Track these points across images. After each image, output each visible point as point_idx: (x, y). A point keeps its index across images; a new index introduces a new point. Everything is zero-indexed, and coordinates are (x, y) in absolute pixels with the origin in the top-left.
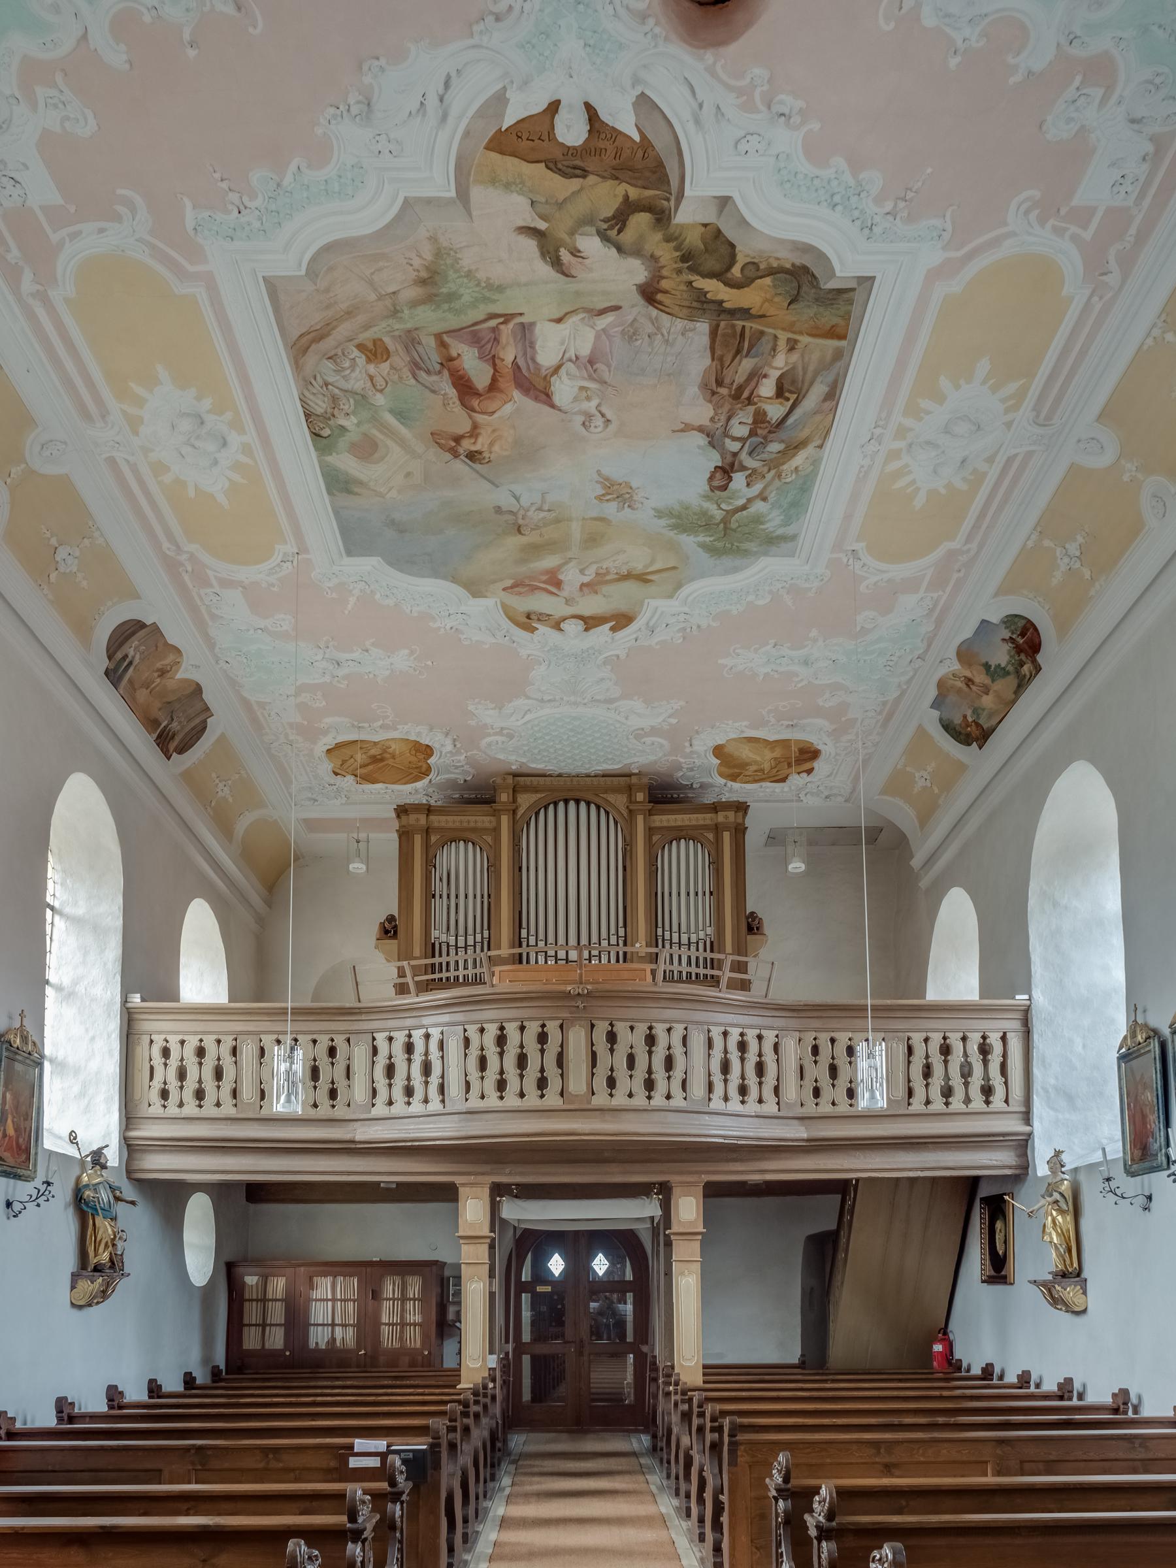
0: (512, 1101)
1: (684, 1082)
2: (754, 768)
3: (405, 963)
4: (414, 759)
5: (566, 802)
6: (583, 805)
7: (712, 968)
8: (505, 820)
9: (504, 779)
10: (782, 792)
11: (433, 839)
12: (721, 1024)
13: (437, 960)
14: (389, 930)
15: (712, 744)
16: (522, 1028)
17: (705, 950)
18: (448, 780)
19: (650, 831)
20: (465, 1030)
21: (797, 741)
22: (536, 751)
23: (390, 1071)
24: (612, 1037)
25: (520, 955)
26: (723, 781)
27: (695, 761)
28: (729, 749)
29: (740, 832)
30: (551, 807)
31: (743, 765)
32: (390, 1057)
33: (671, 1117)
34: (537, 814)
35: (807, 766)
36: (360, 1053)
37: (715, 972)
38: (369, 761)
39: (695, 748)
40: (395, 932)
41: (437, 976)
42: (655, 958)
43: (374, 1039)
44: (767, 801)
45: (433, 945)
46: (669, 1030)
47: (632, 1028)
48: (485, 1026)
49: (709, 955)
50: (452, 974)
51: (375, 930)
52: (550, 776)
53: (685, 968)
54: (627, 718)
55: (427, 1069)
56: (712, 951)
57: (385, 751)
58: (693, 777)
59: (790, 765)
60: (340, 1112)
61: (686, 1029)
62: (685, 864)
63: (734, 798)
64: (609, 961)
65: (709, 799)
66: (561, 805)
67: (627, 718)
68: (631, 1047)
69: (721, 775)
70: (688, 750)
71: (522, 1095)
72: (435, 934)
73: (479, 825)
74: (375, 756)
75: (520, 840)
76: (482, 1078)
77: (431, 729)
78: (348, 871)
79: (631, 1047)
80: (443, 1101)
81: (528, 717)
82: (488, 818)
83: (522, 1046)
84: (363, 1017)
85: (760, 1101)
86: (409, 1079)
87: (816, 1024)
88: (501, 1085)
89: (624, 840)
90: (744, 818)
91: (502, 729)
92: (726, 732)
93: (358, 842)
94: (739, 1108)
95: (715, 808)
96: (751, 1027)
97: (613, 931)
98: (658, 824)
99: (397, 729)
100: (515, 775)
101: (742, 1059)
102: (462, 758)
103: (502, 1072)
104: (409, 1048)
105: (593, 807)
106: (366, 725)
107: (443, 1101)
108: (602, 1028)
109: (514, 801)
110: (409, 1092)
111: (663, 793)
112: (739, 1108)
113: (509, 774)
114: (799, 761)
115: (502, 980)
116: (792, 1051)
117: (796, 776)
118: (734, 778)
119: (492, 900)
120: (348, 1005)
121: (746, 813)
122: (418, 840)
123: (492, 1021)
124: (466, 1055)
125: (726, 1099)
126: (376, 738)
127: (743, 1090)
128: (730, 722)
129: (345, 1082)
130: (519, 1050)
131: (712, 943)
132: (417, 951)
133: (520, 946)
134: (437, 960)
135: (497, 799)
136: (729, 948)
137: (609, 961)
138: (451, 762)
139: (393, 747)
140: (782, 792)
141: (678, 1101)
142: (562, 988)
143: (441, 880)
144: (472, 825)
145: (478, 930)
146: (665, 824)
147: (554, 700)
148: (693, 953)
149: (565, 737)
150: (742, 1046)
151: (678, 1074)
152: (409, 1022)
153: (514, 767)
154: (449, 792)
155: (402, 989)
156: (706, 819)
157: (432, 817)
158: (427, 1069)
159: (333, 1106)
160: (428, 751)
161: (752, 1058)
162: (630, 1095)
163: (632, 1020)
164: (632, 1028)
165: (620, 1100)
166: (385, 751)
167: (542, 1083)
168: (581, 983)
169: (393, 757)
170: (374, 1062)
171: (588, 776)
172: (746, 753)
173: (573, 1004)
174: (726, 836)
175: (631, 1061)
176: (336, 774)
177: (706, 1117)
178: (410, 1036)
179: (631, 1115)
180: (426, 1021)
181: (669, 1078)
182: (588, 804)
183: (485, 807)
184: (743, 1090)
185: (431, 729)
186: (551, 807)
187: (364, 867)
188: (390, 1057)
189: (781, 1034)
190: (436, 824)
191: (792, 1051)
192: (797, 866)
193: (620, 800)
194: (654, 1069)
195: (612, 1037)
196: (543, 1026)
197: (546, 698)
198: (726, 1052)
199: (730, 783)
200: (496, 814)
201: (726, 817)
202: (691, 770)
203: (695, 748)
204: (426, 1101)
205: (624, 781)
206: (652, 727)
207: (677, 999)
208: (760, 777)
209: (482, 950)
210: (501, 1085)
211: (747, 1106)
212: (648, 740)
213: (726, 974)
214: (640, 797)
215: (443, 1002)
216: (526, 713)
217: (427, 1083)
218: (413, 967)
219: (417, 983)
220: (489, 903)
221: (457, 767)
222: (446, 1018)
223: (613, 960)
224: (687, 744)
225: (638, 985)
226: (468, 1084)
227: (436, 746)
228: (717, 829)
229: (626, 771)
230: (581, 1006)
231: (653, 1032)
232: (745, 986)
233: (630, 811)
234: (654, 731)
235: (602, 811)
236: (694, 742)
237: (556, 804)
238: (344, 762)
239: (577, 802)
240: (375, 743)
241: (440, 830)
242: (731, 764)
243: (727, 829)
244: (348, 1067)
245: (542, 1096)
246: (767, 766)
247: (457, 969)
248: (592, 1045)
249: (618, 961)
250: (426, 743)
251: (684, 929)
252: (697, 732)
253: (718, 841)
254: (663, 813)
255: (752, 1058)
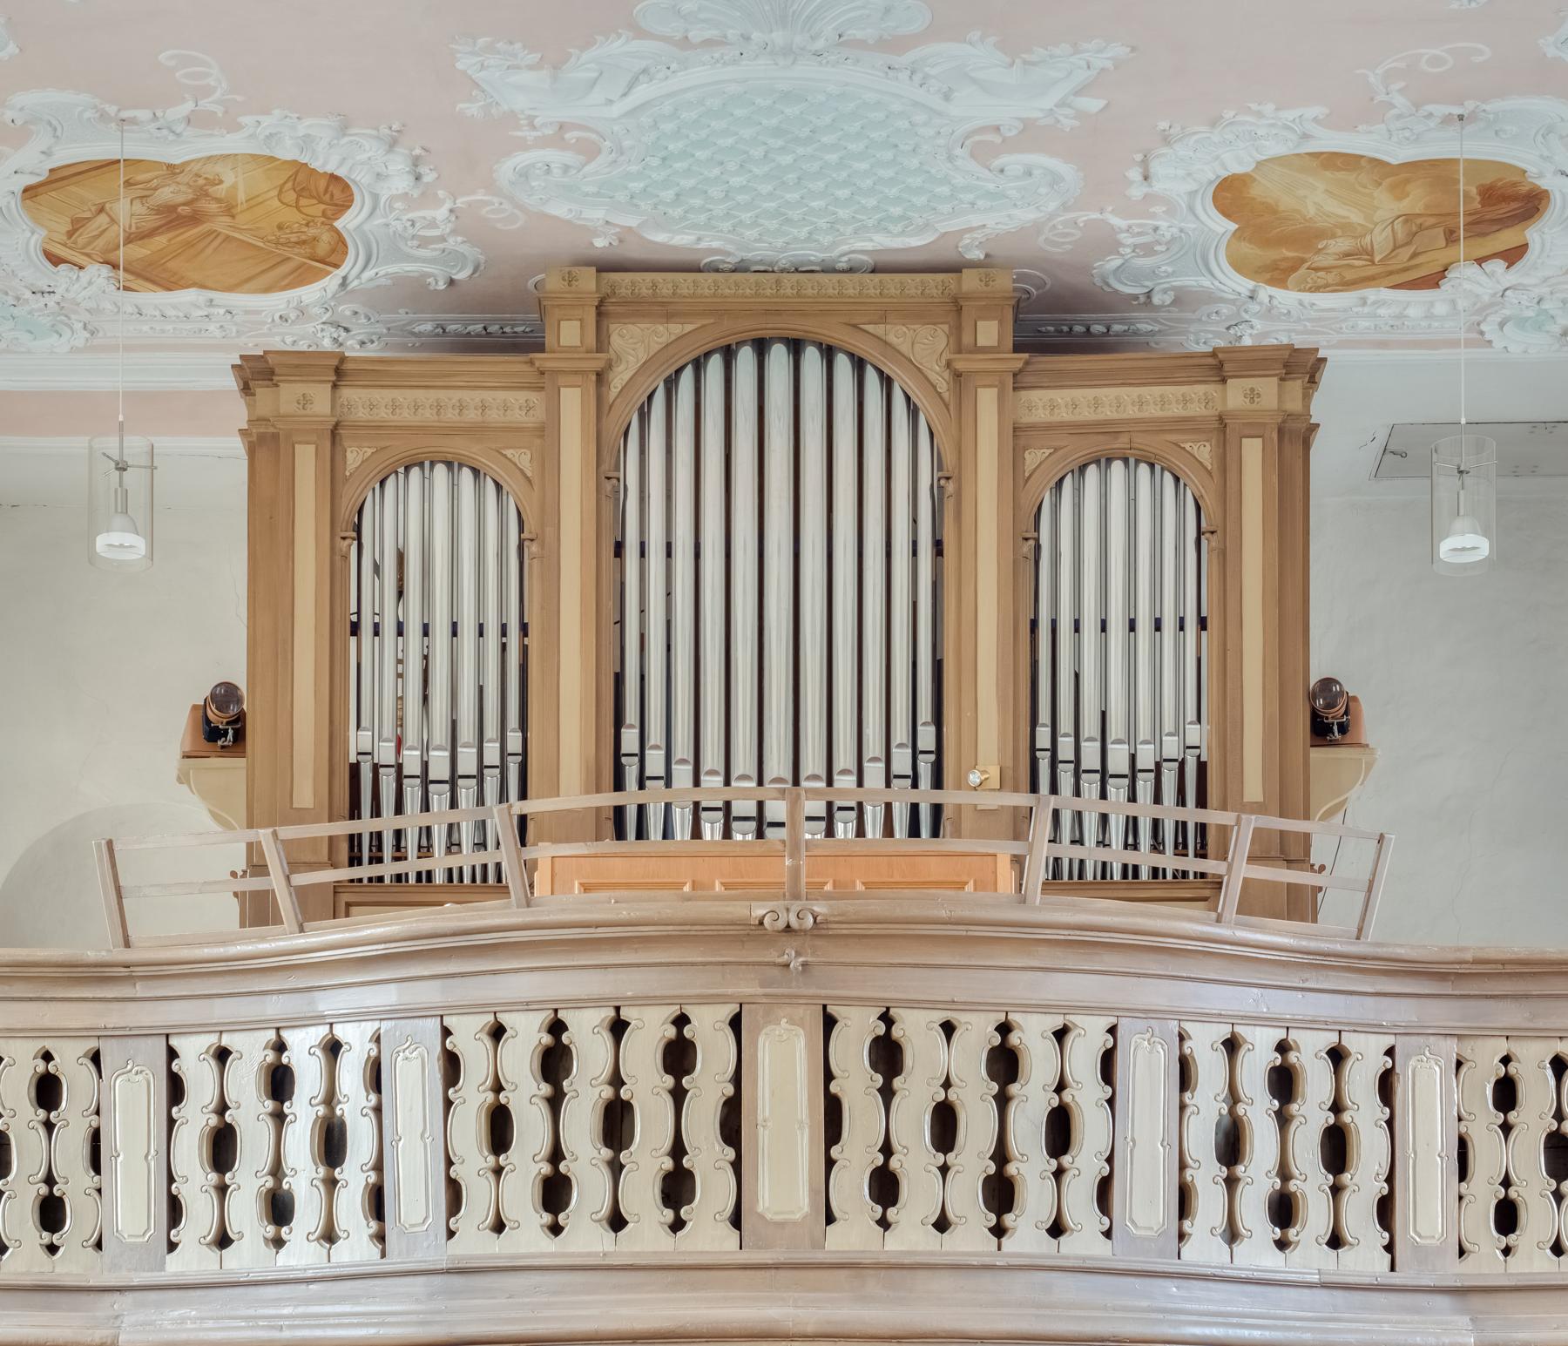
0: (584, 1231)
1: (1104, 1189)
2: (1343, 244)
3: (263, 835)
4: (291, 216)
5: (761, 347)
6: (812, 359)
7: (1202, 854)
8: (573, 403)
9: (570, 279)
10: (1429, 316)
11: (354, 457)
12: (1218, 1018)
13: (365, 825)
14: (222, 728)
15: (1211, 173)
16: (618, 1028)
17: (1181, 801)
18: (399, 281)
19: (1018, 436)
20: (446, 1032)
21: (1473, 165)
22: (668, 195)
23: (222, 1147)
24: (887, 1056)
25: (619, 811)
26: (1244, 285)
27: (1156, 226)
28: (1266, 190)
29: (1294, 440)
30: (715, 365)
31: (1309, 237)
32: (222, 1108)
33: (1067, 1287)
34: (671, 384)
35: (1507, 239)
36: (131, 1098)
37: (1210, 866)
38: (152, 221)
39: (1158, 186)
40: (240, 736)
41: (365, 871)
42: (1019, 824)
43: (172, 1054)
44: (1383, 345)
45: (355, 770)
46: (1061, 1035)
47: (948, 1028)
48: (505, 1019)
49: (1192, 815)
50: (412, 865)
51: (178, 728)
52: (715, 269)
53: (1117, 856)
54: (947, 97)
55: (332, 1143)
56: (1202, 802)
57: (202, 193)
58: (1153, 273)
59: (1451, 237)
60: (74, 1263)
61: (1112, 1031)
62: (1122, 540)
63: (1282, 336)
64: (860, 832)
65: (1202, 339)
66: (745, 359)
67: (947, 97)
68: (947, 1085)
69: (1240, 266)
70: (1137, 192)
71: (617, 1222)
72: (358, 740)
73: (494, 416)
74: (171, 208)
75: (619, 464)
76: (498, 1171)
77: (344, 129)
78: (92, 558)
79: (947, 1085)
80: (380, 1237)
81: (642, 92)
82: (521, 396)
83: (617, 1081)
84: (140, 990)
85: (1335, 1241)
86: (277, 1171)
87: (1511, 1015)
88: (555, 1193)
89: (938, 462)
90: (1307, 398)
91: (562, 127)
92: (1254, 139)
93: (122, 468)
94: (1271, 1261)
95: (1218, 367)
96: (1312, 1025)
97: (901, 733)
98: (1040, 416)
99: (235, 127)
100: (605, 267)
101: (1283, 1119)
102: (441, 213)
103: (556, 1155)
104: (279, 1082)
105: (843, 365)
106: (143, 114)
107: (380, 1237)
108: (857, 1030)
109: (602, 344)
110: (279, 1209)
111: (1058, 324)
112: (1271, 1261)
113: (588, 263)
114: (1479, 226)
115: (568, 881)
116: (1436, 1099)
117: (1472, 270)
118: (1279, 274)
119: (533, 641)
120: (91, 955)
121: (1313, 381)
122: (307, 462)
123: (527, 1006)
124: (448, 1104)
125: (1232, 1235)
126: (176, 154)
127: (1283, 1210)
128: (1269, 108)
129: (88, 1179)
130: (608, 1092)
131: (1202, 767)
132: (306, 794)
133: (619, 785)
134: (365, 825)
135: (549, 341)
136: (1253, 790)
137: (860, 832)
138: (409, 229)
139: (229, 179)
140: (1429, 316)
141: (1085, 1240)
142: (737, 910)
143: (377, 569)
144: (472, 416)
145: (491, 730)
146: (1064, 415)
147: (722, 42)
148: (1145, 810)
149: (757, 152)
150: (1284, 1082)
151: (1085, 1161)
152: (275, 1007)
153: (600, 243)
154: (402, 316)
155: (259, 911)
156: (1194, 400)
157: (348, 393)
158: (332, 1143)
159: (52, 1249)
160: (335, 193)
161: (1312, 1115)
162: (942, 1224)
163: (952, 1004)
164: (948, 1028)
165: (910, 1230)
166: (202, 193)
167: (677, 1188)
168: (796, 896)
169: (229, 210)
170: (171, 1122)
171: (829, 269)
172: (1318, 201)
173: (772, 956)
174: (1253, 453)
175: (945, 1125)
176: (55, 260)
177: (1172, 1287)
178: (280, 1047)
179: (942, 1283)
180: (328, 1003)
181: (1059, 1173)
182: (828, 353)
183: (513, 364)
184: (1283, 1210)
185: (344, 129)
186: (715, 365)
187: (140, 543)
188: (222, 1108)
189: (1401, 1045)
190: (362, 414)
191: (1436, 1099)
192: (1465, 544)
193: (923, 347)
194: (1221, 1189)
195: (887, 1056)
196: (681, 1021)
197: (696, 35)
198: (1234, 1097)
199: (1266, 292)
200: (545, 382)
201: (1253, 395)
202: (1148, 250)
203: (1158, 186)
204: (329, 1236)
205: (938, 283)
206: (1028, 125)
207: (1086, 944)
208: (1361, 270)
209: (503, 796)
210: (555, 1193)
211: (1294, 1255)
212: (1013, 162)
213: (1239, 870)
214: (989, 332)
215: (379, 949)
216: (631, 86)
217: (331, 1183)
218: (288, 846)
219: (303, 896)
220: (524, 651)
221: (424, 242)
222: (388, 996)
223: (873, 829)
224: (1135, 174)
225: (970, 903)
226: (454, 1191)
227: (359, 178)
228: (1223, 429)
229: (946, 255)
230: (795, 964)
231: (1292, 1057)
232: (1299, 904)
233: (958, 375)
234: (1031, 135)
235: (872, 378)
236: (1156, 167)
237: (729, 354)
238: (77, 225)
239: (796, 347)
240: (172, 170)
241: (376, 429)
242: (1271, 236)
243: (1254, 429)
244: (96, 1136)
245: (677, 1225)
246: (1380, 240)
247: (425, 850)
248: (829, 1077)
249: (889, 831)
250: (330, 169)
251: (1116, 729)
252: (1166, 140)
253: (1226, 470)
254: (1060, 380)
255: (1312, 1115)
